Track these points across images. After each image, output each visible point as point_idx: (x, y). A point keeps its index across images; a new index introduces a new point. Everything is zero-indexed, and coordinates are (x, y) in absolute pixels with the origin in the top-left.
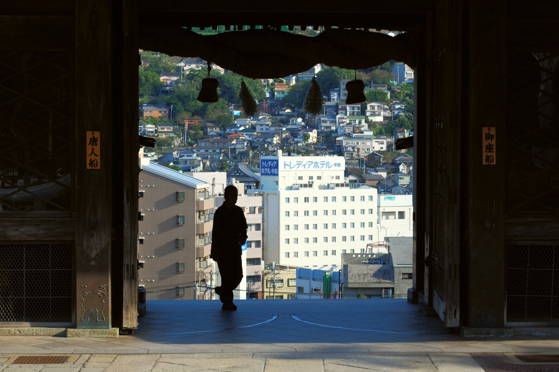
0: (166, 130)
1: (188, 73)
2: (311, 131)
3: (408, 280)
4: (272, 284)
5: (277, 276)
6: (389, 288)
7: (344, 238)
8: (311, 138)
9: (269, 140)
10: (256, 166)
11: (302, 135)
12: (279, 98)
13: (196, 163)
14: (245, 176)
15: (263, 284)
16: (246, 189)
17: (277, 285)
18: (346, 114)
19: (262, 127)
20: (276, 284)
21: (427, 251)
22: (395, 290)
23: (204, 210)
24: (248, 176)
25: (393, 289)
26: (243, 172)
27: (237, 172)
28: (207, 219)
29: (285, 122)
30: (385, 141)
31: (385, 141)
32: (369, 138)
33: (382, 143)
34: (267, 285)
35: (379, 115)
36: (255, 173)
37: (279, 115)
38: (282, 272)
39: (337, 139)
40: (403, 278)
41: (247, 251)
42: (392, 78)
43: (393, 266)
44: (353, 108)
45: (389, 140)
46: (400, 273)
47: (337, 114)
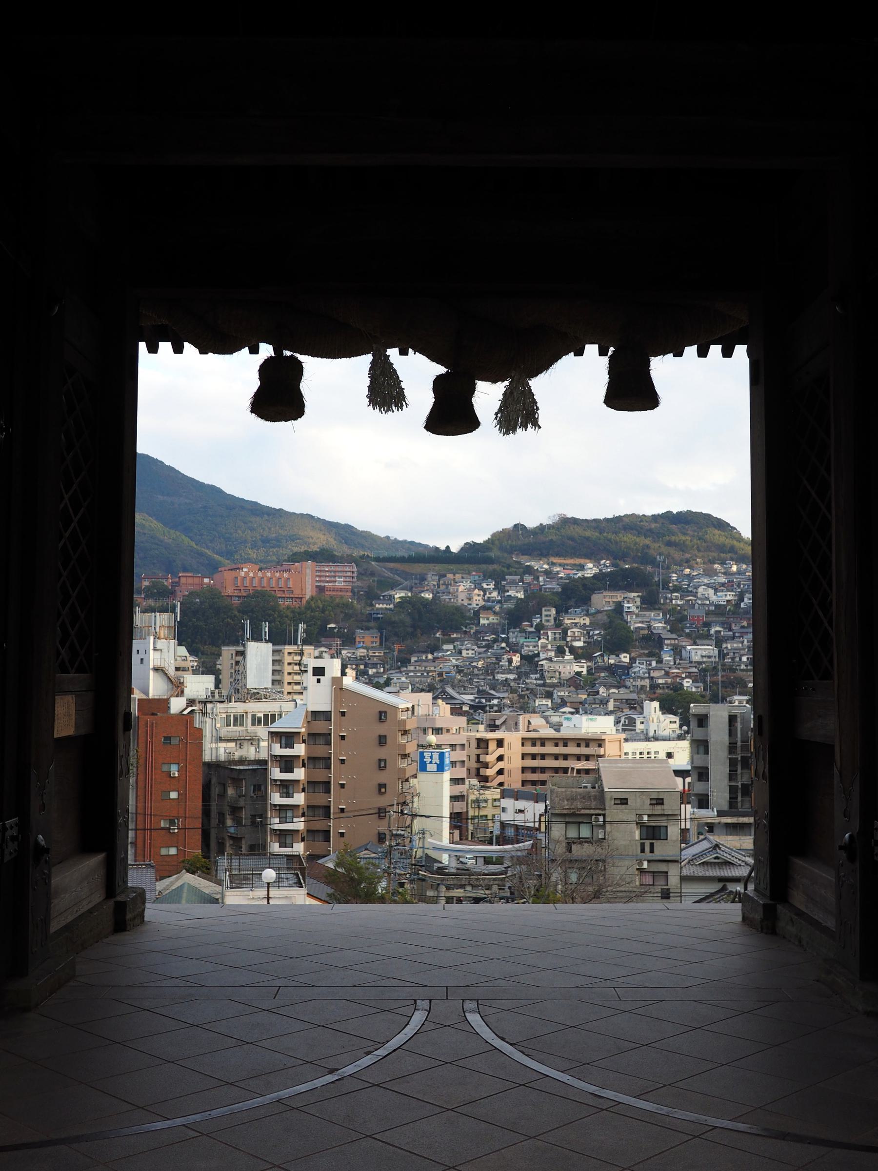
0: (377, 654)
1: (398, 600)
2: (515, 655)
3: (620, 806)
4: (477, 804)
5: (483, 796)
6: (600, 815)
7: (625, 801)
8: (514, 662)
9: (474, 664)
10: (463, 689)
11: (506, 659)
12: (484, 624)
13: (405, 686)
14: (452, 698)
15: (467, 803)
16: (309, 719)
17: (482, 805)
18: (548, 639)
19: (468, 652)
20: (481, 804)
21: (265, 632)
22: (606, 817)
23: (407, 729)
24: (455, 699)
25: (604, 815)
26: (449, 695)
27: (444, 695)
28: (410, 739)
29: (489, 646)
30: (585, 665)
31: (585, 665)
32: (569, 662)
33: (582, 667)
34: (471, 805)
35: (579, 640)
36: (462, 696)
37: (484, 640)
38: (487, 792)
39: (540, 663)
40: (615, 804)
41: (450, 773)
42: (705, 518)
43: (603, 790)
44: (555, 634)
45: (589, 664)
46: (611, 799)
47: (540, 639)
